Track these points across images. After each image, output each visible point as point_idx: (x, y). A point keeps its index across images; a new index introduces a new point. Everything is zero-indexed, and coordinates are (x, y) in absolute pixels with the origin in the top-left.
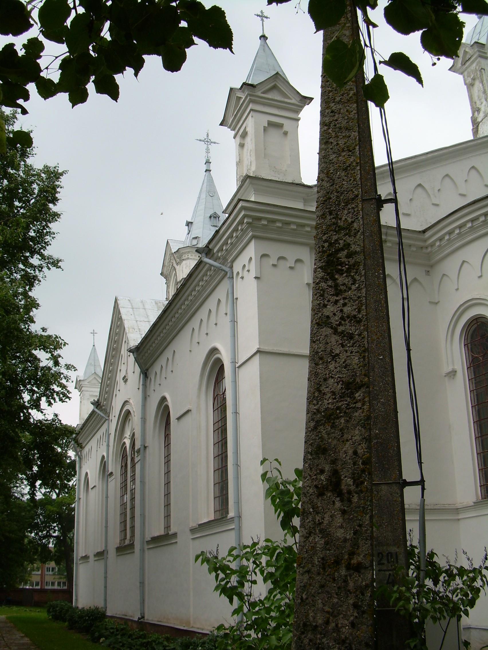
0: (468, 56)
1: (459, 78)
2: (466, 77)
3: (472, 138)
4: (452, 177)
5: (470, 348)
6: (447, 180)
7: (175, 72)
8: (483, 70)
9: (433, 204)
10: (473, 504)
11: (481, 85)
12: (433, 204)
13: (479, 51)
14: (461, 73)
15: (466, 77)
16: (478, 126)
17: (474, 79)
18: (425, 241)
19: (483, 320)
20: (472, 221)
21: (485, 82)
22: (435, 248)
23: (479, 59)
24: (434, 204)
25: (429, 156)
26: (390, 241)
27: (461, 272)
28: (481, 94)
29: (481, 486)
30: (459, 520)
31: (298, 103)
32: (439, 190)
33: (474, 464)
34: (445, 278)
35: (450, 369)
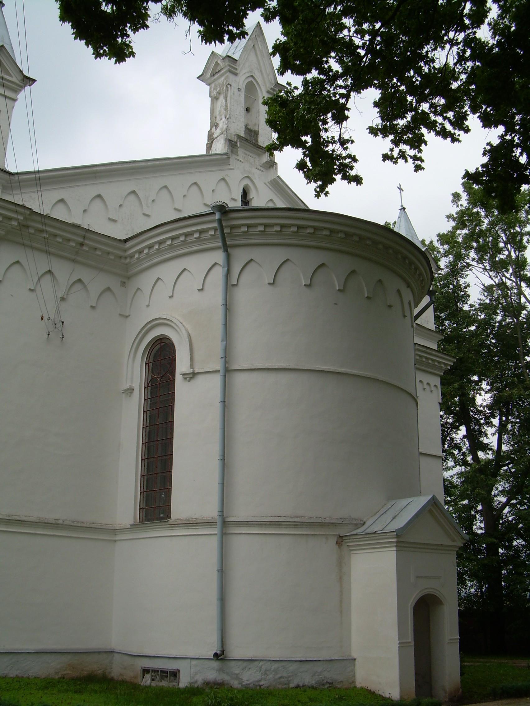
0: (219, 69)
1: (205, 89)
2: (212, 89)
3: (204, 153)
4: (171, 191)
5: (151, 368)
6: (165, 191)
7: (68, 28)
8: (229, 86)
9: (144, 214)
10: (129, 526)
11: (224, 101)
12: (144, 214)
13: (229, 66)
14: (209, 85)
15: (212, 89)
16: (212, 142)
17: (219, 93)
18: (125, 251)
19: (167, 342)
20: (173, 238)
21: (229, 98)
22: (134, 260)
23: (228, 74)
24: (145, 215)
25: (149, 163)
26: (87, 245)
27: (155, 288)
28: (223, 112)
29: (140, 509)
30: (115, 541)
31: (18, 82)
32: (153, 201)
33: (136, 486)
34: (139, 292)
35: (127, 386)
